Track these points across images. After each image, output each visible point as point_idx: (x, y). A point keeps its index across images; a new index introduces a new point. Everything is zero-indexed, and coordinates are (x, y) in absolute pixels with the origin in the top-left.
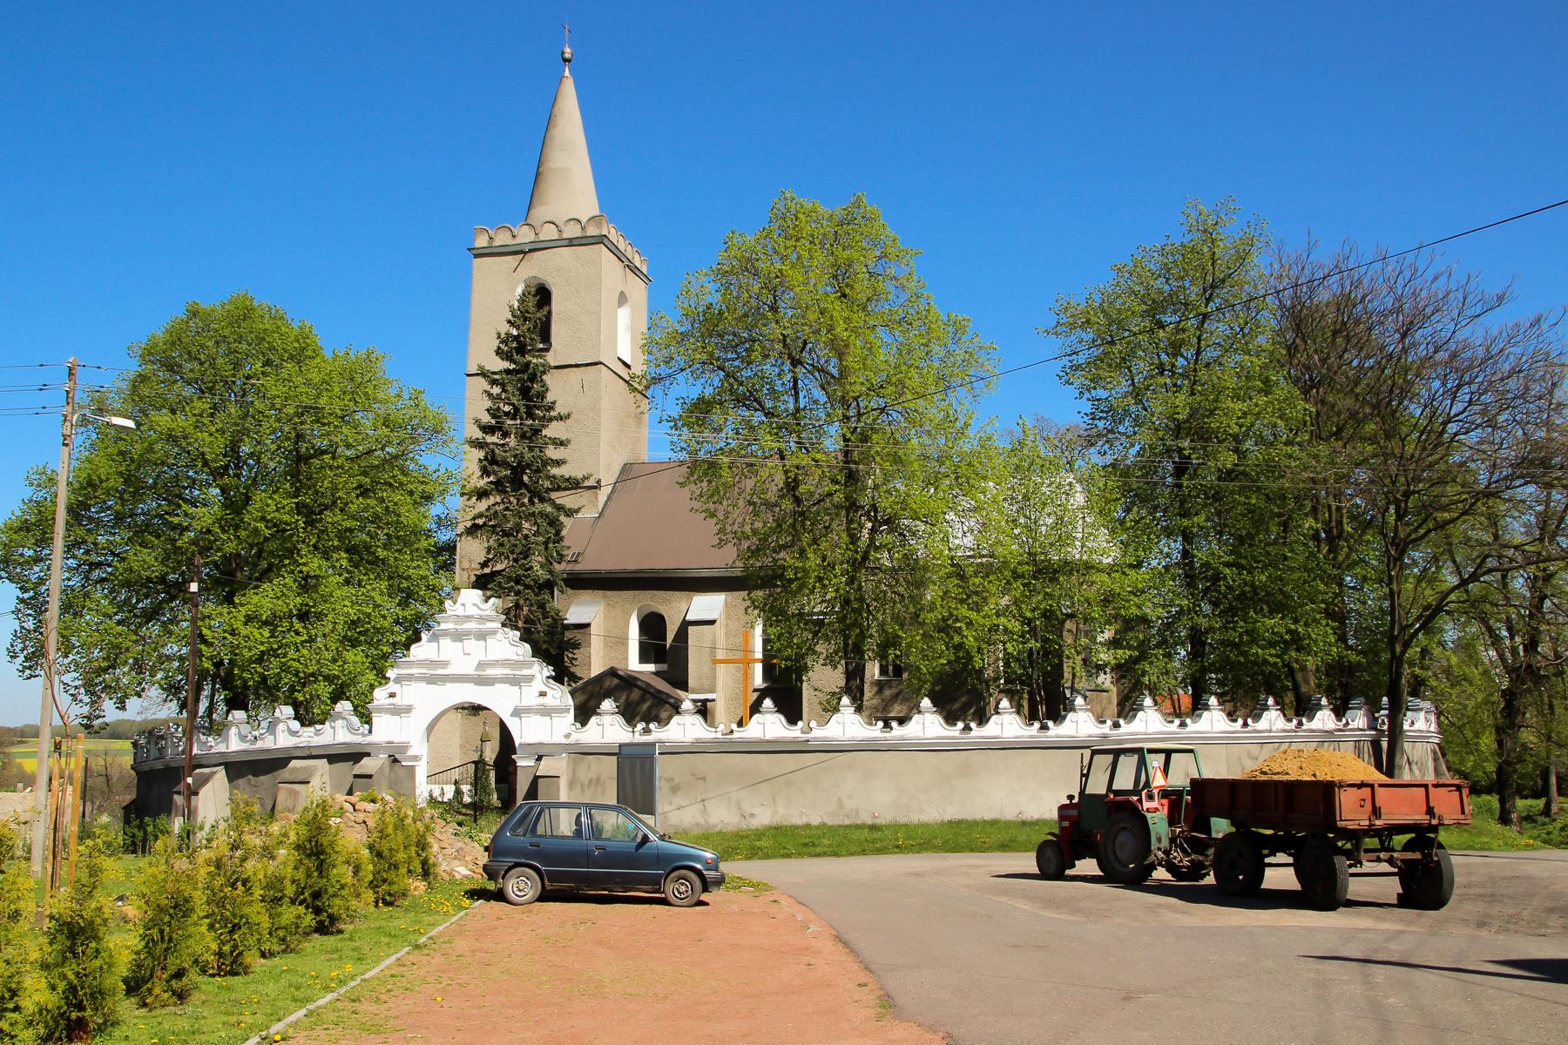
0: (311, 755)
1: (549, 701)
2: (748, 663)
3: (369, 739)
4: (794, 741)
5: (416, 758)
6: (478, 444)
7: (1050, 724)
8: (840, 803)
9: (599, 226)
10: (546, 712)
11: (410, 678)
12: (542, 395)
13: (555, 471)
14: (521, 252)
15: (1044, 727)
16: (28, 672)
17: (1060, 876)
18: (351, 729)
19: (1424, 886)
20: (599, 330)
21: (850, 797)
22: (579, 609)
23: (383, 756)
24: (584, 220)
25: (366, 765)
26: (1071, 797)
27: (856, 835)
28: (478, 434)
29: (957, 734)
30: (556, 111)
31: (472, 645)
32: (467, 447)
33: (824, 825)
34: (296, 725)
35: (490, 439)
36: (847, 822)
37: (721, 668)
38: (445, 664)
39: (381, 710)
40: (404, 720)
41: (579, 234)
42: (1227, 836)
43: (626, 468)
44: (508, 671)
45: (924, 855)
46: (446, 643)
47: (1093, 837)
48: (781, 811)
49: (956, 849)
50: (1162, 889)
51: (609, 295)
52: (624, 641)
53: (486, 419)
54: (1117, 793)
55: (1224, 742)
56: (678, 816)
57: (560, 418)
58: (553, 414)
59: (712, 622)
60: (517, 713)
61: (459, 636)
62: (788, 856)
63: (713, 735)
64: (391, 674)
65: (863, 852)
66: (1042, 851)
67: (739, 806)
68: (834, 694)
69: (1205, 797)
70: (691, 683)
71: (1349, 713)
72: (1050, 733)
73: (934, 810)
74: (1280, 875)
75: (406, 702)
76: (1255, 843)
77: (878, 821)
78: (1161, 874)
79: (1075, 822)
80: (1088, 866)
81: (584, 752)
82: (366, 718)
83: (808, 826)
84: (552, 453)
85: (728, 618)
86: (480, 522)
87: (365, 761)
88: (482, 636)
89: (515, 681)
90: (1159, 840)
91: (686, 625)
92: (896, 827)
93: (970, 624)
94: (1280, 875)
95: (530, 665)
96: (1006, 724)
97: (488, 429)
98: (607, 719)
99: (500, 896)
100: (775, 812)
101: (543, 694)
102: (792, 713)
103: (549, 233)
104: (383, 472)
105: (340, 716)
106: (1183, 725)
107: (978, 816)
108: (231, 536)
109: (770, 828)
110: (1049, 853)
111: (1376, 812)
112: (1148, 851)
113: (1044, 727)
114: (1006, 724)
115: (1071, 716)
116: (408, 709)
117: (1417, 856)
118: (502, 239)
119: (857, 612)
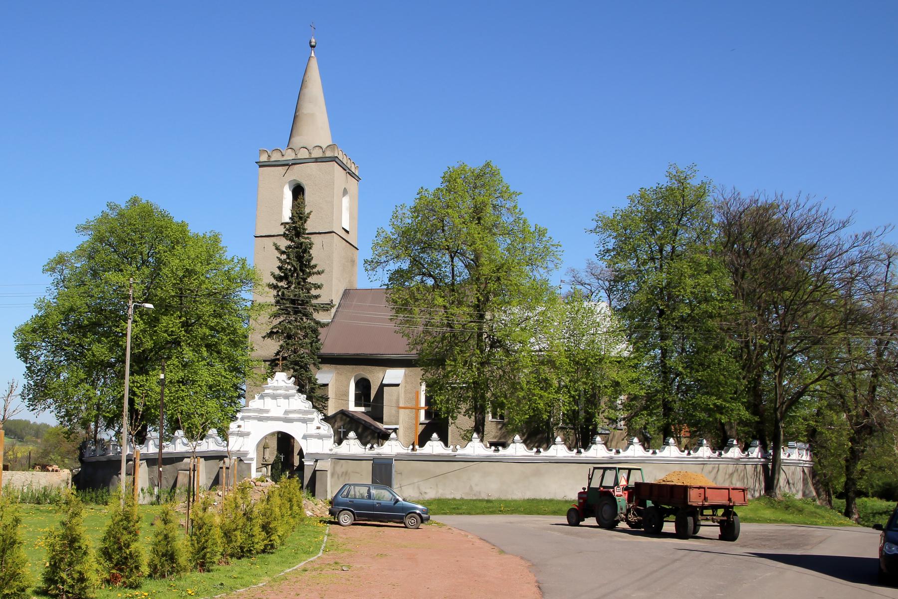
0: (194, 455)
2: (418, 409)
4: (448, 456)
5: (252, 459)
6: (275, 287)
7: (582, 450)
8: (471, 488)
9: (333, 151)
10: (320, 437)
11: (249, 418)
12: (309, 261)
13: (314, 302)
14: (287, 165)
15: (579, 452)
16: (31, 408)
17: (577, 525)
18: (217, 444)
19: (729, 532)
20: (332, 213)
21: (477, 485)
22: (325, 376)
24: (324, 147)
26: (584, 489)
27: (479, 504)
28: (275, 282)
29: (533, 454)
30: (307, 78)
31: (281, 401)
32: (267, 289)
33: (462, 499)
34: (185, 440)
35: (280, 284)
36: (474, 498)
37: (401, 411)
38: (267, 411)
39: (232, 434)
40: (246, 440)
41: (321, 155)
42: (650, 507)
43: (346, 293)
44: (300, 416)
45: (514, 515)
46: (268, 400)
47: (594, 506)
48: (441, 491)
49: (530, 512)
50: (624, 531)
51: (338, 190)
52: (347, 394)
53: (277, 272)
54: (604, 487)
55: (668, 462)
56: (407, 490)
57: (319, 273)
58: (315, 270)
59: (398, 385)
60: (305, 437)
61: (274, 397)
62: (445, 514)
63: (406, 451)
64: (239, 415)
65: (483, 513)
66: (569, 514)
67: (419, 488)
68: (468, 431)
69: (638, 492)
70: (385, 419)
71: (750, 449)
72: (582, 455)
73: (520, 493)
74: (669, 527)
76: (661, 509)
77: (490, 498)
78: (623, 525)
79: (585, 500)
80: (592, 521)
81: (339, 458)
82: (225, 438)
83: (454, 499)
84: (314, 292)
85: (406, 382)
86: (275, 330)
88: (287, 397)
89: (305, 421)
90: (622, 509)
91: (382, 386)
92: (500, 501)
93: (541, 397)
94: (669, 527)
95: (312, 413)
96: (559, 450)
97: (280, 279)
98: (352, 442)
99: (338, 523)
100: (437, 492)
101: (318, 428)
102: (444, 439)
103: (303, 154)
104: (222, 302)
105: (211, 436)
106: (654, 453)
107: (543, 497)
108: (135, 333)
109: (435, 500)
110: (573, 514)
111: (705, 499)
112: (616, 514)
113: (579, 452)
114: (559, 450)
115: (593, 446)
116: (248, 434)
117: (725, 518)
118: (276, 157)
119: (477, 381)
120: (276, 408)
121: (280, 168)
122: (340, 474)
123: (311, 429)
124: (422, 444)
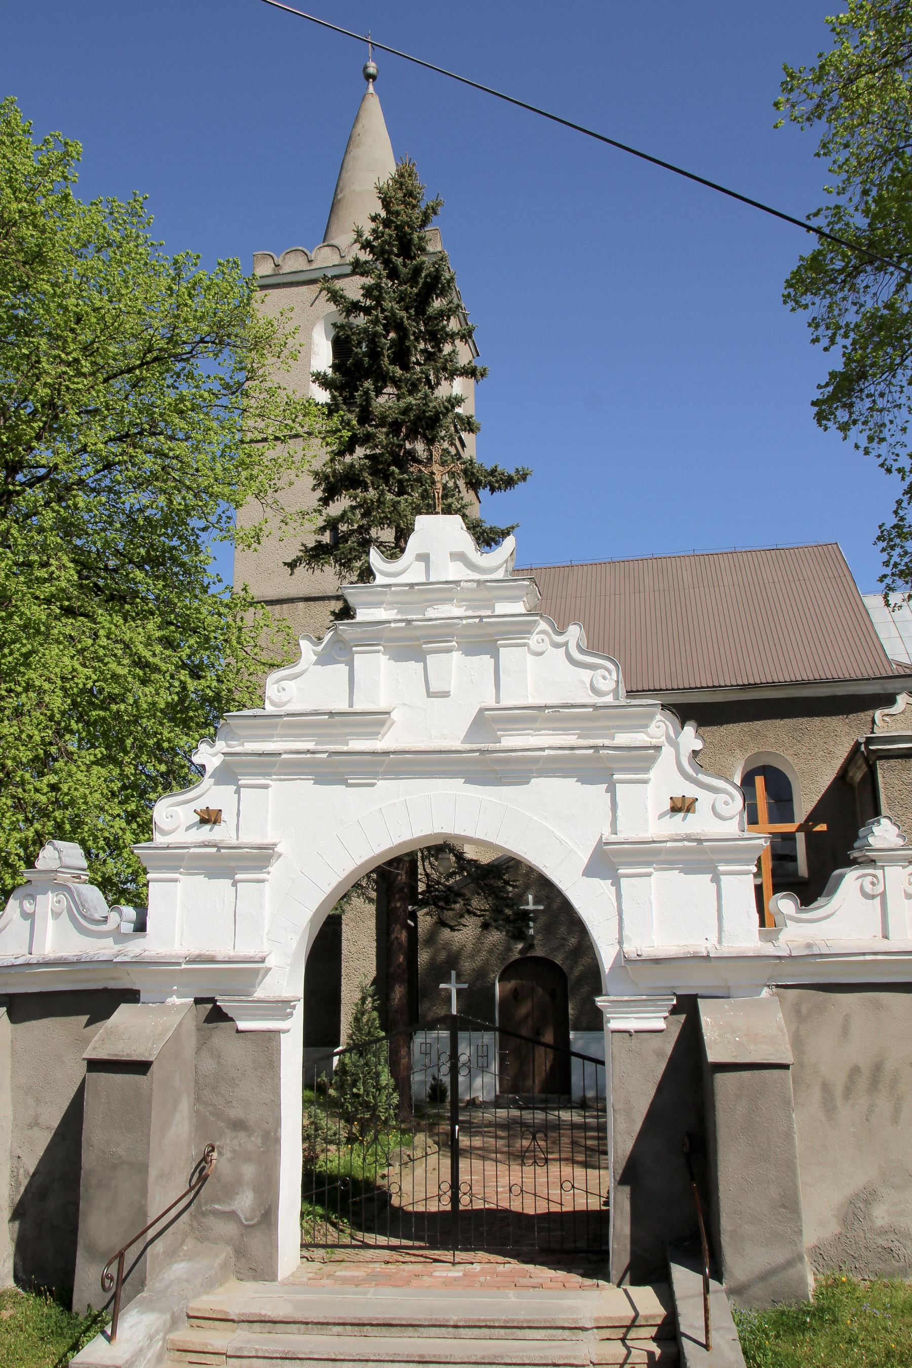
1: (701, 823)
3: (136, 948)
10: (699, 858)
11: (267, 765)
18: (81, 919)
23: (180, 1001)
25: (127, 1031)
38: (376, 720)
39: (179, 861)
61: (411, 644)
64: (208, 755)
75: (250, 837)
87: (123, 1014)
88: (484, 640)
89: (597, 769)
101: (681, 806)
116: (262, 857)
118: (293, 264)
120: (415, 700)
121: (304, 289)
122: (839, 1081)
123: (643, 810)
124: (810, 889)
